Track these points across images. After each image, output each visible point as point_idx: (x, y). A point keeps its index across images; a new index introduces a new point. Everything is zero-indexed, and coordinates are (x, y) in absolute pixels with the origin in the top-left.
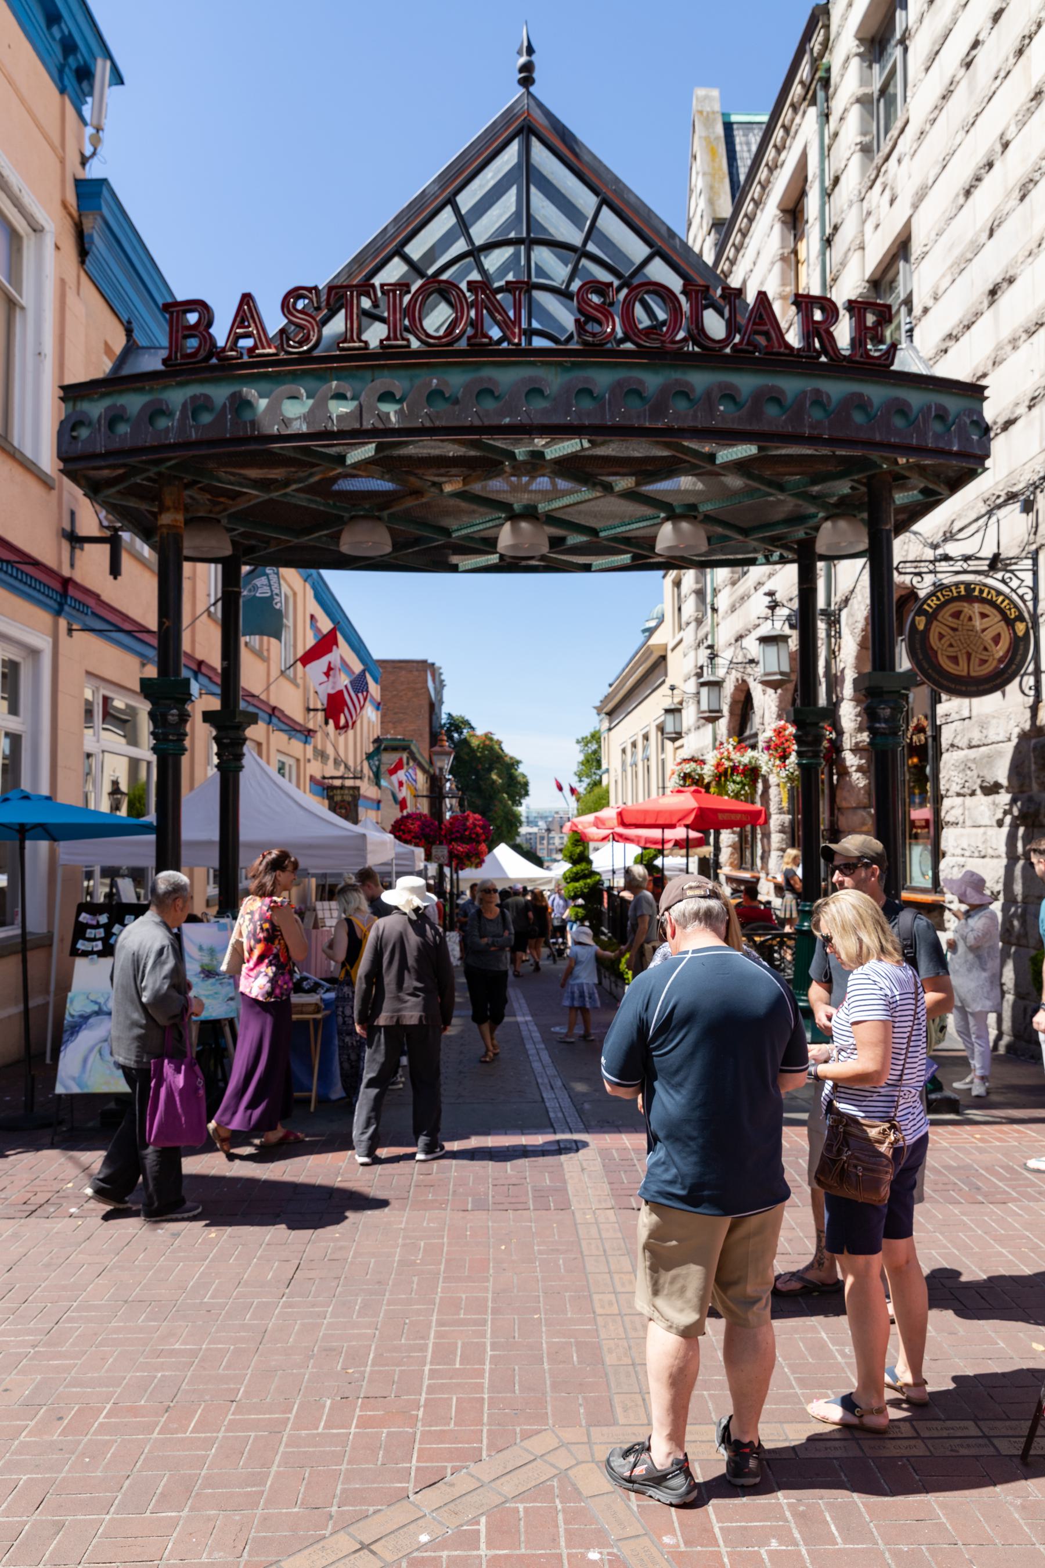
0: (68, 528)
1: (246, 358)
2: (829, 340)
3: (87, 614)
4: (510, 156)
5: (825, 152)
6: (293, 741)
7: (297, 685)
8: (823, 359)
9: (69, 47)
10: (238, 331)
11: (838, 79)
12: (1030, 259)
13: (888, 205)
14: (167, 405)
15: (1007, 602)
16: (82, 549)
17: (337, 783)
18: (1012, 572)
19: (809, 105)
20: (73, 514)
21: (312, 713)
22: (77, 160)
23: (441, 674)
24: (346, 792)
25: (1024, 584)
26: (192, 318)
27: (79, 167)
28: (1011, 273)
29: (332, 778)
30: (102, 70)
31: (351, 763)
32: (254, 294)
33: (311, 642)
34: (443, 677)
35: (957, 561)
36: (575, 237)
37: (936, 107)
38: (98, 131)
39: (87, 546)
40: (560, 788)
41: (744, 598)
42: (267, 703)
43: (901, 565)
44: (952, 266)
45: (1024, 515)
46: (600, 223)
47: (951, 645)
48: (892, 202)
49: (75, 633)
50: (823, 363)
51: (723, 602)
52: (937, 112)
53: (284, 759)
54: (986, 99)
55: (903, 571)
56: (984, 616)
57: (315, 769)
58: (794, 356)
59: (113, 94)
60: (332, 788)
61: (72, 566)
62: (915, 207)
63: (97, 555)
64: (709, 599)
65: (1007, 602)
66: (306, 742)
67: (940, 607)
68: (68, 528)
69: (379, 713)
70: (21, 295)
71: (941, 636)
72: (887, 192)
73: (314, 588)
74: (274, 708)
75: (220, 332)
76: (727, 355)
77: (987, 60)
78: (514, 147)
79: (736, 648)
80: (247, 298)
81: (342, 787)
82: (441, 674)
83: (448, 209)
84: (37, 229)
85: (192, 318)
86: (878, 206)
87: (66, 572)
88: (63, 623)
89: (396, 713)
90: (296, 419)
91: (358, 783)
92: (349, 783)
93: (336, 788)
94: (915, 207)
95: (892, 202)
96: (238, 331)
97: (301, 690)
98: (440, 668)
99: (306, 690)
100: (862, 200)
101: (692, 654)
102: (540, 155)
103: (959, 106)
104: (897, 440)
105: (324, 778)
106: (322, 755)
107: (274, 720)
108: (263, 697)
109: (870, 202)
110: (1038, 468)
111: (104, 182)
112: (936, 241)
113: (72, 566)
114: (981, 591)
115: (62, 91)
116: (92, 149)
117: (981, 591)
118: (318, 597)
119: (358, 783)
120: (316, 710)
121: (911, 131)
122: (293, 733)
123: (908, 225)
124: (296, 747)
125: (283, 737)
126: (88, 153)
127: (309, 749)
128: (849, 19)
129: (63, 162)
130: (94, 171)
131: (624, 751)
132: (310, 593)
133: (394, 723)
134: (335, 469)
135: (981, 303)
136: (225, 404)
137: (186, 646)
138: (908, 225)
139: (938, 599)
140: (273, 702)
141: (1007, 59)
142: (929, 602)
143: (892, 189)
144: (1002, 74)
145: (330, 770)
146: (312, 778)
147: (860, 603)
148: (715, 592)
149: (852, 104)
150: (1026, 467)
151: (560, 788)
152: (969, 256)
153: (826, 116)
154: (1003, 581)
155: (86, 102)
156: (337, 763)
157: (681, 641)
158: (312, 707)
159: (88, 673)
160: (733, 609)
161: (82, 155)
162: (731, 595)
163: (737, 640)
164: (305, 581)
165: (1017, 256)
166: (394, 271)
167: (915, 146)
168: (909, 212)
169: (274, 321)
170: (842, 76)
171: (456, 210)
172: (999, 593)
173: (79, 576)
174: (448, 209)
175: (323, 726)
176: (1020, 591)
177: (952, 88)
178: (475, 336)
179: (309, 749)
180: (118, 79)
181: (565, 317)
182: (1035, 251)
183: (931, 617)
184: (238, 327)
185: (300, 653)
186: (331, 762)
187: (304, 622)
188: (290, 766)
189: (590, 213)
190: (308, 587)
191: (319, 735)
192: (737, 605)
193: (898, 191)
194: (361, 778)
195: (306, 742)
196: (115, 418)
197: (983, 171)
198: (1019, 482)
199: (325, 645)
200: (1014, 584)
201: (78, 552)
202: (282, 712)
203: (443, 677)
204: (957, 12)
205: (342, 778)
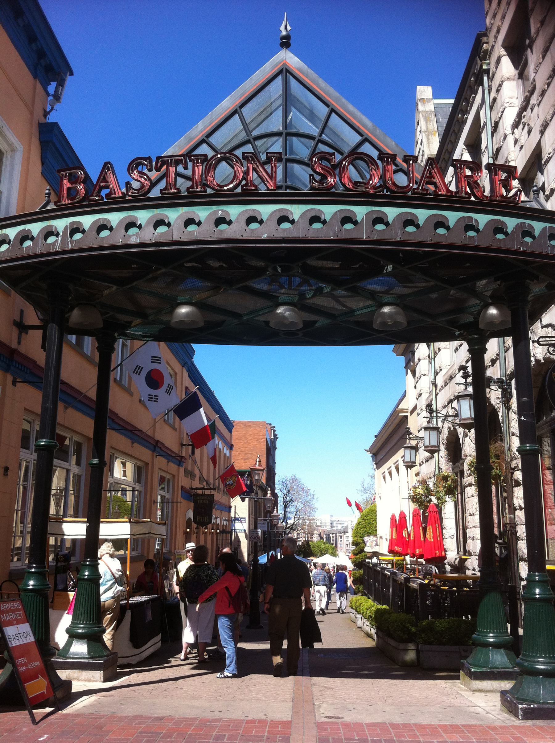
0: (18, 319)
1: (105, 200)
2: (474, 184)
3: (26, 373)
6: (170, 464)
7: (175, 429)
8: (473, 199)
9: (41, 54)
10: (102, 184)
14: (56, 228)
16: (27, 333)
17: (200, 492)
20: (22, 311)
22: (41, 113)
24: (205, 498)
27: (43, 118)
29: (197, 489)
31: (211, 481)
36: (314, 131)
39: (30, 331)
40: (349, 504)
42: (153, 439)
43: (541, 340)
46: (330, 123)
49: (18, 384)
50: (472, 201)
53: (164, 474)
55: (541, 343)
57: (184, 482)
58: (453, 197)
60: (196, 495)
61: (19, 343)
62: (542, 133)
66: (179, 465)
68: (18, 319)
72: (526, 127)
73: (188, 371)
74: (157, 442)
81: (203, 495)
84: (13, 150)
87: (14, 345)
88: (10, 378)
89: (246, 454)
90: (133, 235)
91: (213, 492)
92: (207, 492)
93: (199, 495)
94: (542, 133)
96: (102, 184)
97: (177, 432)
99: (180, 433)
104: (525, 249)
105: (192, 488)
106: (190, 474)
107: (158, 450)
111: (56, 124)
113: (19, 343)
115: (35, 76)
119: (213, 492)
122: (170, 458)
123: (539, 145)
124: (172, 467)
125: (163, 461)
126: (48, 110)
127: (182, 470)
128: (499, 38)
129: (32, 113)
130: (51, 119)
132: (186, 374)
133: (245, 460)
134: (160, 269)
137: (109, 406)
138: (539, 145)
140: (158, 437)
143: (528, 125)
145: (196, 484)
146: (182, 487)
151: (349, 504)
156: (201, 479)
158: (184, 443)
159: (26, 409)
161: (45, 111)
163: (448, 404)
164: (183, 366)
167: (540, 99)
170: (497, 68)
173: (22, 349)
178: (246, 185)
179: (182, 470)
180: (72, 74)
186: (197, 479)
187: (182, 391)
188: (169, 480)
189: (323, 117)
190: (185, 370)
191: (190, 461)
192: (448, 382)
193: (532, 125)
194: (214, 489)
195: (179, 465)
201: (23, 335)
202: (163, 444)
203: (276, 433)
205: (203, 489)
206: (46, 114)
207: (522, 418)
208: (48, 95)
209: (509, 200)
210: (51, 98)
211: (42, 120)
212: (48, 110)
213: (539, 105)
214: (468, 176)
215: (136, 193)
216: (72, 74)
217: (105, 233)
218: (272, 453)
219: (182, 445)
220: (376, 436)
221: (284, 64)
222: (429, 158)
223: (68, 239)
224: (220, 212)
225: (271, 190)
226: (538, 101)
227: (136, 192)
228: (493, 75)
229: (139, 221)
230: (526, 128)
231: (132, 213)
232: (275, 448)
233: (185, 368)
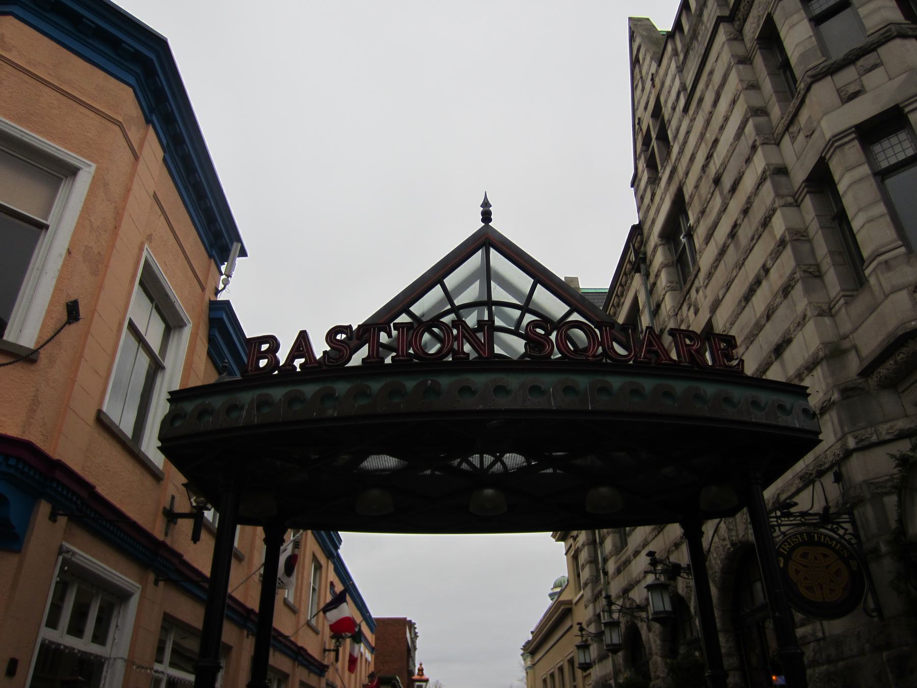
4: (476, 259)
5: (650, 292)
10: (296, 353)
11: (651, 257)
12: (799, 328)
13: (694, 315)
15: (839, 545)
18: (838, 523)
19: (635, 273)
21: (327, 653)
22: (213, 291)
23: (415, 628)
25: (848, 532)
26: (265, 347)
28: (788, 337)
30: (236, 247)
32: (307, 331)
33: (329, 598)
34: (416, 630)
35: (796, 516)
37: (716, 260)
38: (228, 277)
39: (180, 521)
41: (627, 563)
44: (745, 340)
45: (836, 484)
47: (806, 578)
48: (696, 313)
51: (611, 567)
52: (717, 263)
54: (748, 251)
56: (825, 556)
59: (239, 260)
63: (186, 526)
64: (600, 566)
65: (839, 545)
67: (792, 550)
68: (168, 507)
69: (373, 656)
70: (164, 362)
71: (797, 572)
73: (334, 563)
75: (282, 356)
76: (630, 365)
77: (744, 234)
78: (479, 254)
79: (624, 599)
80: (303, 336)
82: (415, 628)
83: (439, 286)
85: (265, 347)
86: (687, 316)
87: (160, 536)
95: (696, 313)
98: (415, 624)
100: (677, 315)
101: (591, 606)
102: (496, 259)
103: (731, 256)
108: (292, 639)
109: (682, 315)
110: (837, 452)
112: (731, 328)
114: (819, 538)
115: (211, 256)
116: (223, 286)
117: (819, 538)
118: (337, 571)
120: (329, 650)
121: (702, 275)
126: (220, 289)
130: (221, 297)
131: (545, 681)
132: (331, 567)
135: (770, 357)
136: (281, 399)
139: (789, 544)
141: (758, 229)
142: (783, 546)
144: (756, 237)
147: (715, 559)
148: (605, 560)
149: (662, 268)
150: (828, 452)
152: (755, 332)
153: (647, 275)
154: (832, 530)
155: (224, 264)
157: (582, 596)
160: (619, 571)
162: (616, 562)
165: (789, 327)
166: (404, 318)
168: (708, 316)
169: (319, 347)
171: (444, 287)
172: (832, 539)
174: (439, 286)
175: (334, 663)
176: (847, 537)
177: (725, 249)
180: (243, 253)
181: (519, 345)
182: (802, 322)
183: (787, 558)
184: (295, 351)
185: (322, 605)
187: (326, 586)
189: (527, 290)
191: (331, 670)
192: (622, 568)
196: (203, 413)
197: (754, 286)
198: (825, 463)
199: (338, 600)
200: (841, 532)
203: (416, 630)
204: (720, 214)
206: (217, 292)
207: (777, 614)
208: (221, 274)
209: (733, 369)
210: (223, 277)
211: (213, 299)
212: (220, 289)
213: (706, 287)
214: (687, 345)
215: (333, 363)
216: (243, 253)
217: (297, 407)
218: (412, 655)
219: (325, 650)
220: (532, 633)
221: (487, 238)
222: (647, 327)
223: (254, 412)
224: (429, 381)
225: (485, 358)
226: (705, 284)
227: (335, 361)
228: (651, 263)
229: (337, 392)
230: (692, 309)
231: (329, 385)
232: (415, 649)
233: (331, 561)
